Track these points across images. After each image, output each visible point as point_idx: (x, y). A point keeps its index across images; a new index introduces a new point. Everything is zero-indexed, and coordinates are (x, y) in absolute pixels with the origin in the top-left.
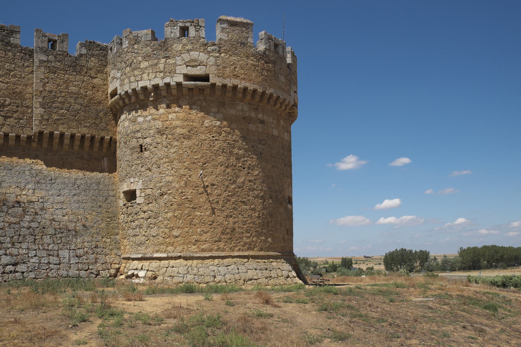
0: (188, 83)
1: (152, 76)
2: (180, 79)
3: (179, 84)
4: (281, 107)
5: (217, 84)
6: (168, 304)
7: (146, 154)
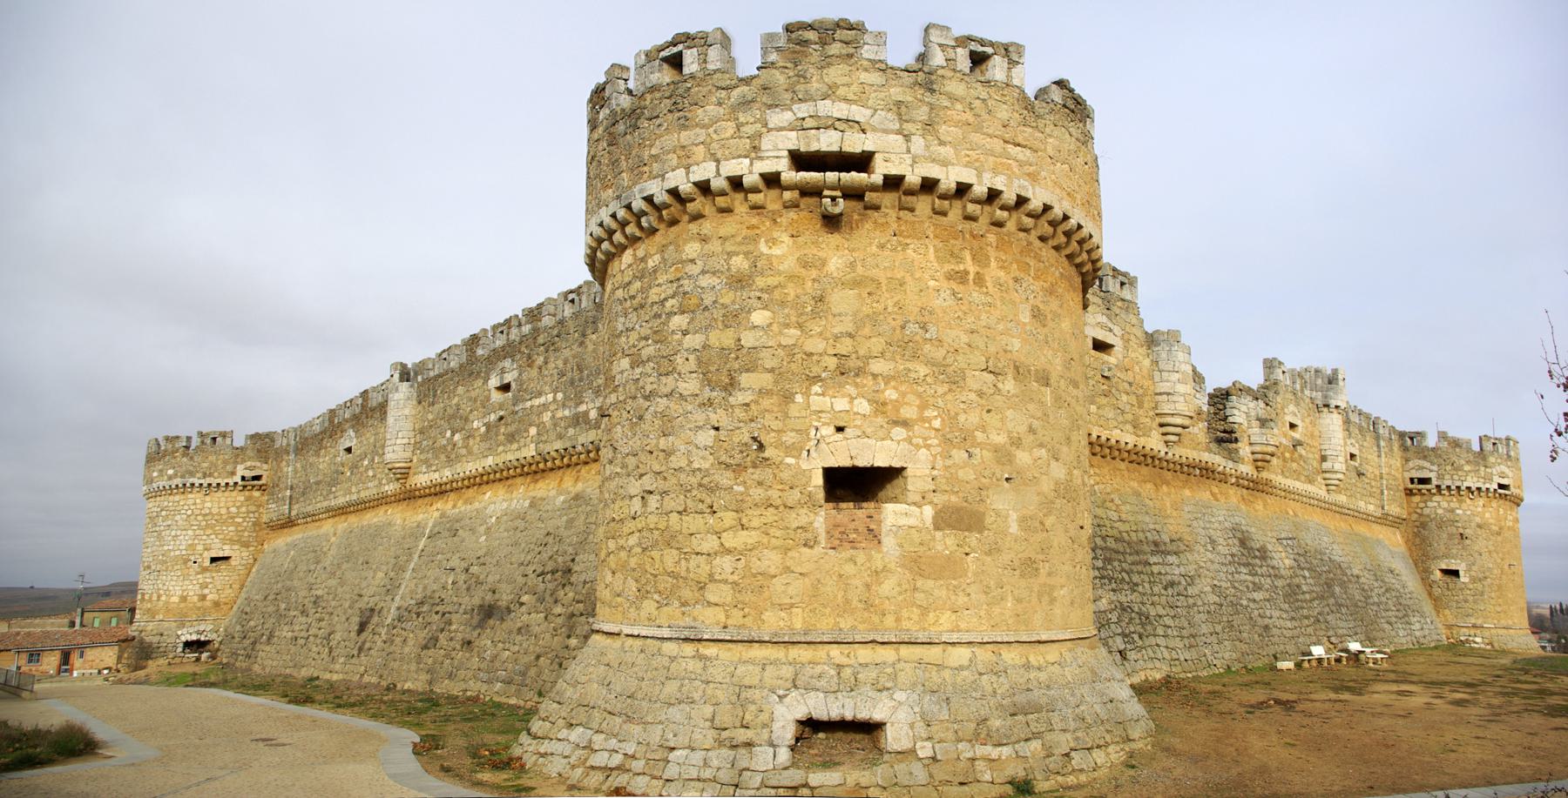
1: (1475, 479)
7: (1468, 542)
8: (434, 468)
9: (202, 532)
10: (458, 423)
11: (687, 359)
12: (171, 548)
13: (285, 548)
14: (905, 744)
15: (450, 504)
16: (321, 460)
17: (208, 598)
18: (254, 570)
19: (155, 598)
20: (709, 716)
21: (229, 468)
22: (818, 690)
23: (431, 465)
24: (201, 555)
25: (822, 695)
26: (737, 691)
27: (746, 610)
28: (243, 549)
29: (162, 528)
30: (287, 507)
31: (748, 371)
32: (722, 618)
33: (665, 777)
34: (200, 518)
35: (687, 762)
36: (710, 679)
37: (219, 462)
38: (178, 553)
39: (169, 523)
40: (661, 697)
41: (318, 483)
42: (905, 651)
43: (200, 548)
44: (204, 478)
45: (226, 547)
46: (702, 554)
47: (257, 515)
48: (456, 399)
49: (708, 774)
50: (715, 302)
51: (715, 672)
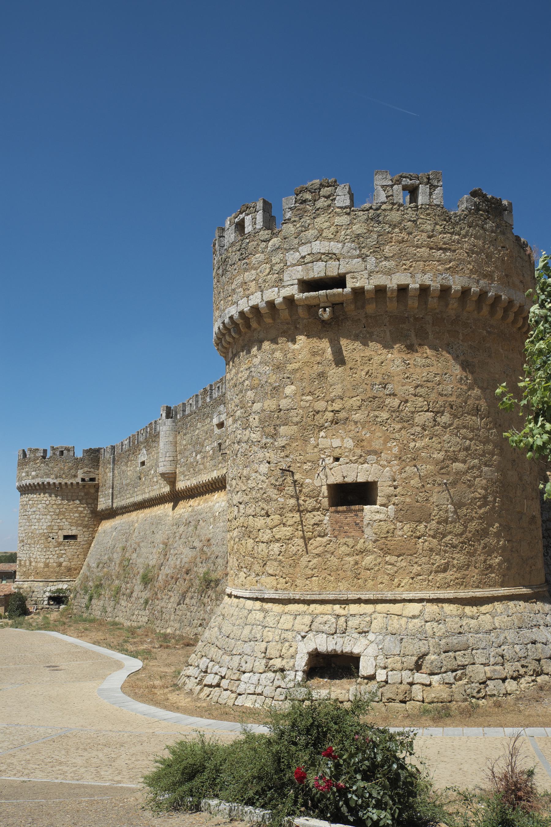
0: (306, 294)
2: (293, 290)
3: (289, 301)
4: (505, 317)
5: (388, 286)
6: (191, 644)
8: (187, 477)
9: (57, 517)
10: (198, 447)
11: (254, 419)
12: (36, 527)
13: (110, 530)
14: (371, 672)
15: (196, 504)
16: (129, 469)
17: (64, 564)
18: (92, 545)
19: (28, 564)
20: (263, 650)
21: (73, 472)
22: (323, 632)
23: (185, 476)
24: (57, 533)
25: (325, 636)
26: (280, 633)
27: (287, 579)
28: (84, 530)
29: (30, 513)
30: (110, 501)
31: (284, 425)
32: (275, 583)
33: (238, 692)
34: (55, 506)
35: (250, 681)
36: (267, 625)
37: (66, 468)
38: (41, 531)
39: (34, 509)
40: (242, 637)
41: (127, 485)
42: (379, 607)
43: (55, 527)
44: (56, 478)
45: (73, 528)
46: (264, 542)
47: (93, 506)
48: (197, 431)
49: (259, 690)
50: (266, 382)
51: (269, 620)
